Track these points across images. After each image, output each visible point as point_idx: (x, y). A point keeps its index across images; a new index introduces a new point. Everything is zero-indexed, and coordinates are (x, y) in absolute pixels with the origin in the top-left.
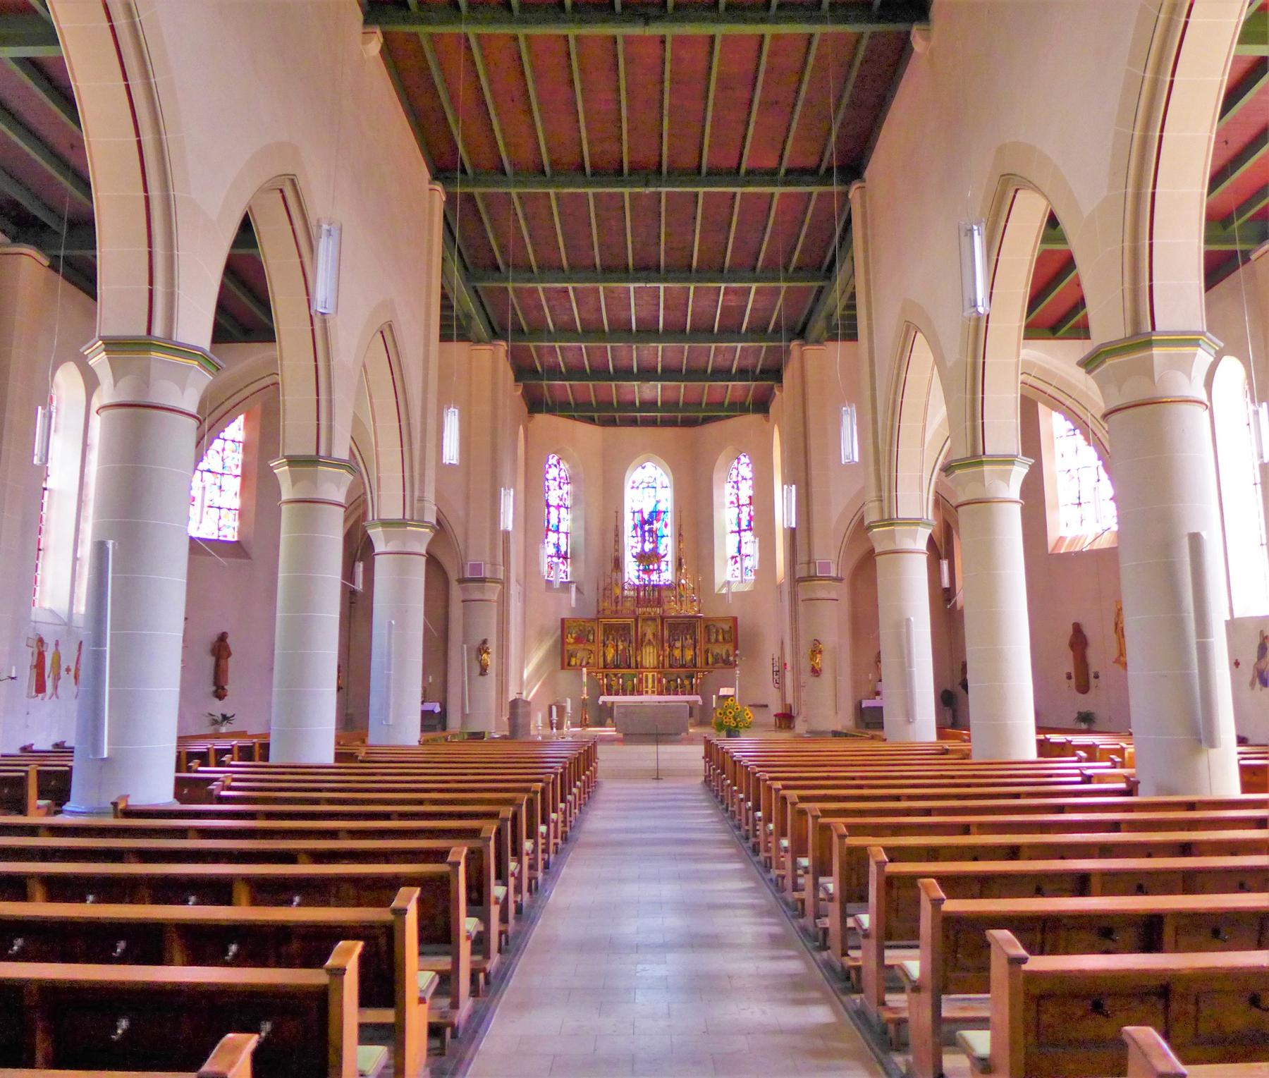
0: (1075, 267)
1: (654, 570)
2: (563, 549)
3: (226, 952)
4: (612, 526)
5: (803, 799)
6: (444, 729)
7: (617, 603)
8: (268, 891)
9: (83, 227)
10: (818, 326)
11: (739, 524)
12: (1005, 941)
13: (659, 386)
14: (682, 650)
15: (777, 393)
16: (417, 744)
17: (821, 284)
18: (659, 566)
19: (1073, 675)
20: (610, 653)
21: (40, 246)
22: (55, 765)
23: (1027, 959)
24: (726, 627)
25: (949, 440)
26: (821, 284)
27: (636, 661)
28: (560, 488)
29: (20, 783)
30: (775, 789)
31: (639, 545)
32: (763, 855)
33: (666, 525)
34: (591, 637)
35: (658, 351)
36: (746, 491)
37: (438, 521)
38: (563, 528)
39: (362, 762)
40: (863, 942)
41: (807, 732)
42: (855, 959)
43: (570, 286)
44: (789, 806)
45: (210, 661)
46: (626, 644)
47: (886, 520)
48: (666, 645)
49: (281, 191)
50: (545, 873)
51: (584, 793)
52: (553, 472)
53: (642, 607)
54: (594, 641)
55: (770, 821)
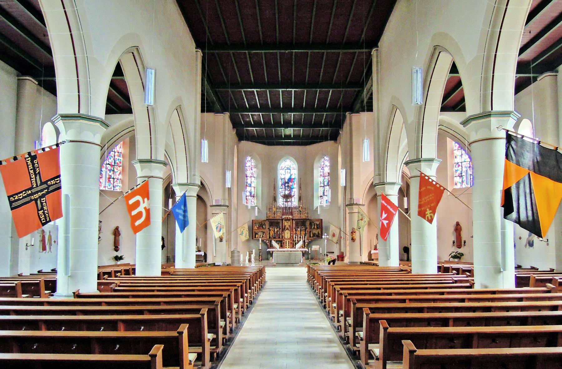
0: (462, 85)
1: (289, 201)
2: (253, 193)
3: (141, 329)
4: (272, 184)
5: (342, 289)
6: (206, 261)
7: (274, 214)
8: (132, 325)
9: (50, 70)
10: (358, 106)
11: (324, 183)
12: (408, 345)
13: (292, 130)
14: (301, 232)
15: (340, 132)
16: (194, 268)
17: (359, 89)
18: (291, 200)
19: (455, 242)
20: (272, 233)
21: (34, 76)
22: (50, 278)
23: (416, 351)
24: (318, 223)
25: (408, 153)
26: (359, 89)
27: (282, 236)
28: (252, 170)
29: (37, 285)
30: (332, 285)
31: (284, 192)
32: (327, 309)
33: (295, 184)
34: (264, 227)
35: (291, 116)
36: (327, 170)
37: (201, 182)
38: (253, 185)
39: (172, 275)
40: (361, 342)
41: (349, 262)
42: (358, 348)
43: (255, 90)
44: (336, 292)
45: (112, 237)
47: (381, 183)
49: (133, 53)
50: (242, 316)
51: (259, 286)
52: (248, 164)
53: (285, 215)
54: (265, 228)
55: (330, 297)
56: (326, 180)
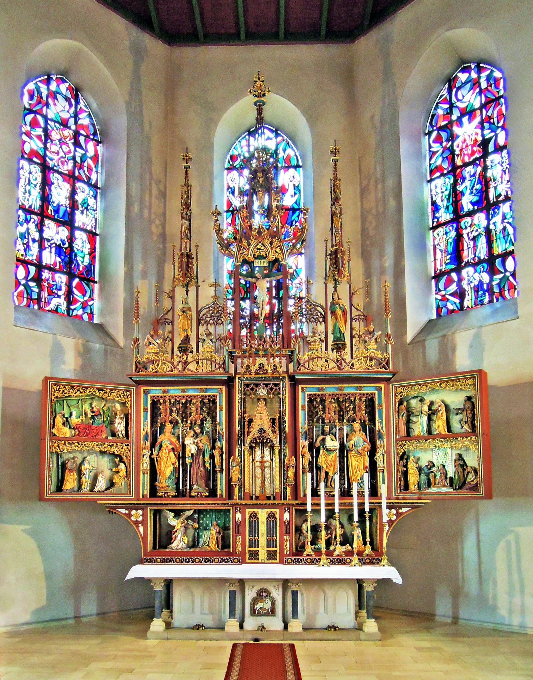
15: (95, 630)
28: (77, 144)
46: (205, 442)
48: (303, 443)
54: (127, 435)
56: (467, 183)
